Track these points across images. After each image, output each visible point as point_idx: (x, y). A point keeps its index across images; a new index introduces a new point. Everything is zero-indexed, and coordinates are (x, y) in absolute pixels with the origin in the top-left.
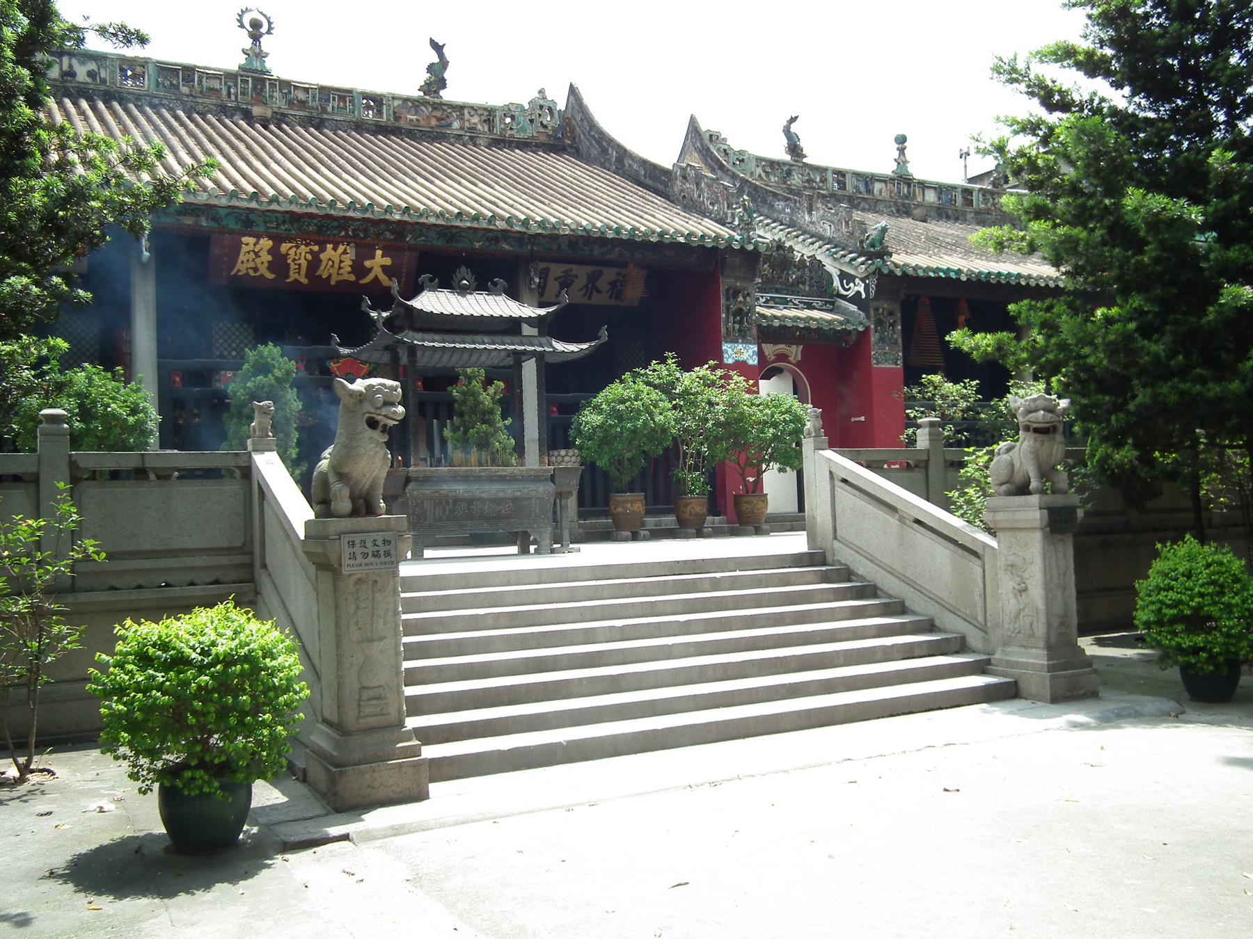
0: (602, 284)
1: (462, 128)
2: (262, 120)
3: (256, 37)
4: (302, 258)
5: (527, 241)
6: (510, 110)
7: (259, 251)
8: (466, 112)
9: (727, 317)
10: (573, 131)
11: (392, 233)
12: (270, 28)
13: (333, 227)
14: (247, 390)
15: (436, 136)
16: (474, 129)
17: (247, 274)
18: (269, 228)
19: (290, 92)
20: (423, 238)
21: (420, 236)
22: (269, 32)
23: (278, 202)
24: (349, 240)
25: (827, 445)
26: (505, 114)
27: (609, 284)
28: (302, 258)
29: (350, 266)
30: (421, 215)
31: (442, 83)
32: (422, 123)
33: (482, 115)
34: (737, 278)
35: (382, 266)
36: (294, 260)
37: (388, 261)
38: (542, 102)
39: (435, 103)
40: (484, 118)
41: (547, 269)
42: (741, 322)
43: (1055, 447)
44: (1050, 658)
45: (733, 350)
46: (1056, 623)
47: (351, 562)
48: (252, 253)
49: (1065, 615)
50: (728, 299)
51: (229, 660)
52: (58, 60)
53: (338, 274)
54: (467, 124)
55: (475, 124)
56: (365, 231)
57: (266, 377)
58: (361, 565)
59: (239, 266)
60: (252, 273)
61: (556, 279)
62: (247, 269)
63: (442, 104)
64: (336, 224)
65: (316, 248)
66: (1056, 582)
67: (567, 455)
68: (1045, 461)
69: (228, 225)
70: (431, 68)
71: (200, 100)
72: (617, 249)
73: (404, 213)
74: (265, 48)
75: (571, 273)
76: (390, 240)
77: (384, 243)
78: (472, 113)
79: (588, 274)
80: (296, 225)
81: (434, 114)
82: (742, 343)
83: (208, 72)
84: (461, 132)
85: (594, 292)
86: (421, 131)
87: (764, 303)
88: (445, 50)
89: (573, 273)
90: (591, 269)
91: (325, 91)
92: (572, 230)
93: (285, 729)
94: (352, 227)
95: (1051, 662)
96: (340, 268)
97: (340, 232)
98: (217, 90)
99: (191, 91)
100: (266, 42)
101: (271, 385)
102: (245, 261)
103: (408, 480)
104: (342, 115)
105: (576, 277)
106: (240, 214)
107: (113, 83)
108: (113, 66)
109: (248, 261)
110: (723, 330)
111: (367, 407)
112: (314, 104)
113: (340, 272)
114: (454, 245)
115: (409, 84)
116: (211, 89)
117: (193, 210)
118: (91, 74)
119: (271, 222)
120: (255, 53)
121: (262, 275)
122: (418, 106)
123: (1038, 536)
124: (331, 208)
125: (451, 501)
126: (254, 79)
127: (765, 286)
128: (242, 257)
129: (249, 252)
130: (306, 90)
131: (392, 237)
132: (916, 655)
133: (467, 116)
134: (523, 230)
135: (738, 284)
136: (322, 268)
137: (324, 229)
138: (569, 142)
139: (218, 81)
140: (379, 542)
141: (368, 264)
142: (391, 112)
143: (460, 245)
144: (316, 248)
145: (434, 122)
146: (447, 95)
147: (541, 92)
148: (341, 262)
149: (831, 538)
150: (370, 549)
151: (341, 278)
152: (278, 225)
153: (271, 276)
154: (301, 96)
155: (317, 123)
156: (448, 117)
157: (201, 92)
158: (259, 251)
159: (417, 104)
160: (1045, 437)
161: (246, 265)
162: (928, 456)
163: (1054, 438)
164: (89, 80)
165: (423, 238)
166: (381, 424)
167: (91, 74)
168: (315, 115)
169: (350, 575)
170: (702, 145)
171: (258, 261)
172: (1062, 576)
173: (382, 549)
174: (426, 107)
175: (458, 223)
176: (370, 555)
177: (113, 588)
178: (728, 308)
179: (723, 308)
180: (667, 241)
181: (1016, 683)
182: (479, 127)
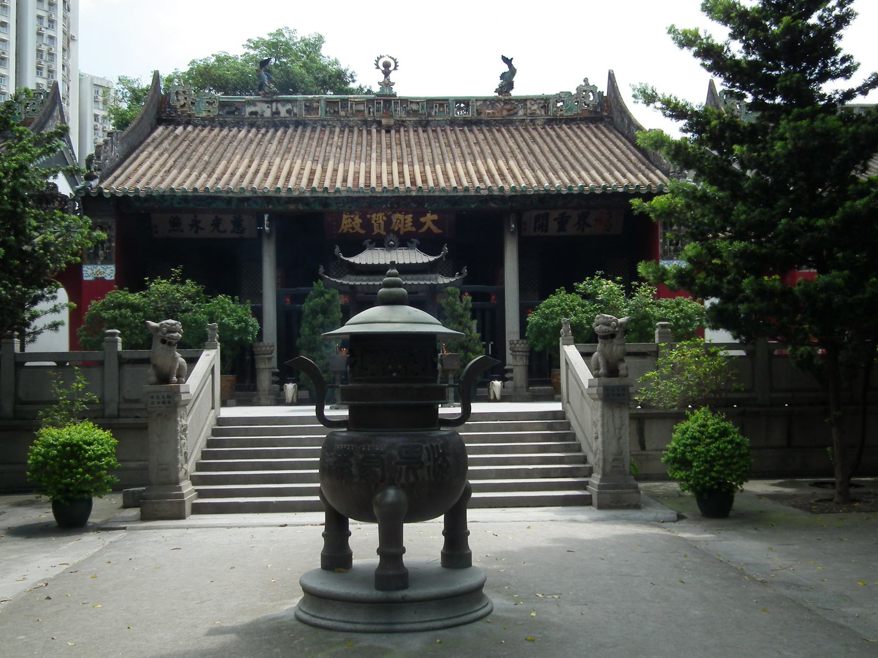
1: (525, 115)
2: (387, 127)
3: (387, 73)
4: (381, 219)
6: (560, 97)
8: (528, 103)
10: (609, 107)
12: (396, 66)
15: (507, 123)
16: (534, 113)
17: (348, 232)
19: (407, 106)
20: (436, 205)
22: (395, 69)
25: (573, 341)
26: (556, 101)
28: (381, 219)
31: (510, 85)
32: (497, 114)
33: (540, 103)
36: (376, 221)
38: (585, 88)
39: (505, 100)
40: (542, 105)
46: (610, 458)
47: (152, 406)
48: (349, 219)
49: (620, 453)
51: (64, 445)
52: (270, 106)
53: (404, 227)
54: (529, 111)
55: (535, 110)
57: (320, 299)
58: (156, 407)
59: (343, 227)
60: (351, 231)
61: (555, 220)
62: (348, 229)
63: (510, 100)
67: (523, 343)
70: (503, 76)
71: (351, 119)
74: (392, 80)
78: (533, 102)
81: (505, 107)
82: (677, 260)
83: (356, 100)
84: (525, 118)
86: (495, 120)
88: (513, 63)
91: (430, 102)
92: (535, 191)
93: (91, 475)
94: (389, 202)
95: (602, 484)
96: (405, 224)
98: (361, 111)
99: (346, 114)
100: (393, 77)
104: (441, 117)
107: (300, 115)
108: (300, 105)
110: (660, 251)
111: (160, 333)
112: (423, 112)
113: (406, 226)
115: (488, 88)
116: (358, 111)
118: (289, 112)
120: (385, 84)
121: (357, 232)
122: (494, 103)
126: (385, 101)
129: (348, 218)
130: (418, 103)
131: (416, 206)
132: (552, 476)
133: (529, 105)
134: (502, 194)
138: (606, 114)
139: (363, 105)
141: (422, 220)
142: (475, 110)
145: (505, 113)
146: (514, 93)
147: (586, 80)
148: (405, 220)
150: (161, 400)
151: (406, 230)
152: (344, 206)
154: (415, 107)
155: (424, 124)
156: (515, 108)
157: (352, 114)
159: (493, 102)
161: (347, 226)
163: (612, 342)
164: (287, 115)
165: (436, 205)
166: (168, 341)
167: (289, 112)
168: (424, 119)
169: (154, 412)
170: (715, 103)
171: (354, 223)
172: (617, 431)
173: (167, 400)
174: (499, 103)
177: (137, 417)
179: (660, 235)
180: (609, 192)
182: (538, 112)
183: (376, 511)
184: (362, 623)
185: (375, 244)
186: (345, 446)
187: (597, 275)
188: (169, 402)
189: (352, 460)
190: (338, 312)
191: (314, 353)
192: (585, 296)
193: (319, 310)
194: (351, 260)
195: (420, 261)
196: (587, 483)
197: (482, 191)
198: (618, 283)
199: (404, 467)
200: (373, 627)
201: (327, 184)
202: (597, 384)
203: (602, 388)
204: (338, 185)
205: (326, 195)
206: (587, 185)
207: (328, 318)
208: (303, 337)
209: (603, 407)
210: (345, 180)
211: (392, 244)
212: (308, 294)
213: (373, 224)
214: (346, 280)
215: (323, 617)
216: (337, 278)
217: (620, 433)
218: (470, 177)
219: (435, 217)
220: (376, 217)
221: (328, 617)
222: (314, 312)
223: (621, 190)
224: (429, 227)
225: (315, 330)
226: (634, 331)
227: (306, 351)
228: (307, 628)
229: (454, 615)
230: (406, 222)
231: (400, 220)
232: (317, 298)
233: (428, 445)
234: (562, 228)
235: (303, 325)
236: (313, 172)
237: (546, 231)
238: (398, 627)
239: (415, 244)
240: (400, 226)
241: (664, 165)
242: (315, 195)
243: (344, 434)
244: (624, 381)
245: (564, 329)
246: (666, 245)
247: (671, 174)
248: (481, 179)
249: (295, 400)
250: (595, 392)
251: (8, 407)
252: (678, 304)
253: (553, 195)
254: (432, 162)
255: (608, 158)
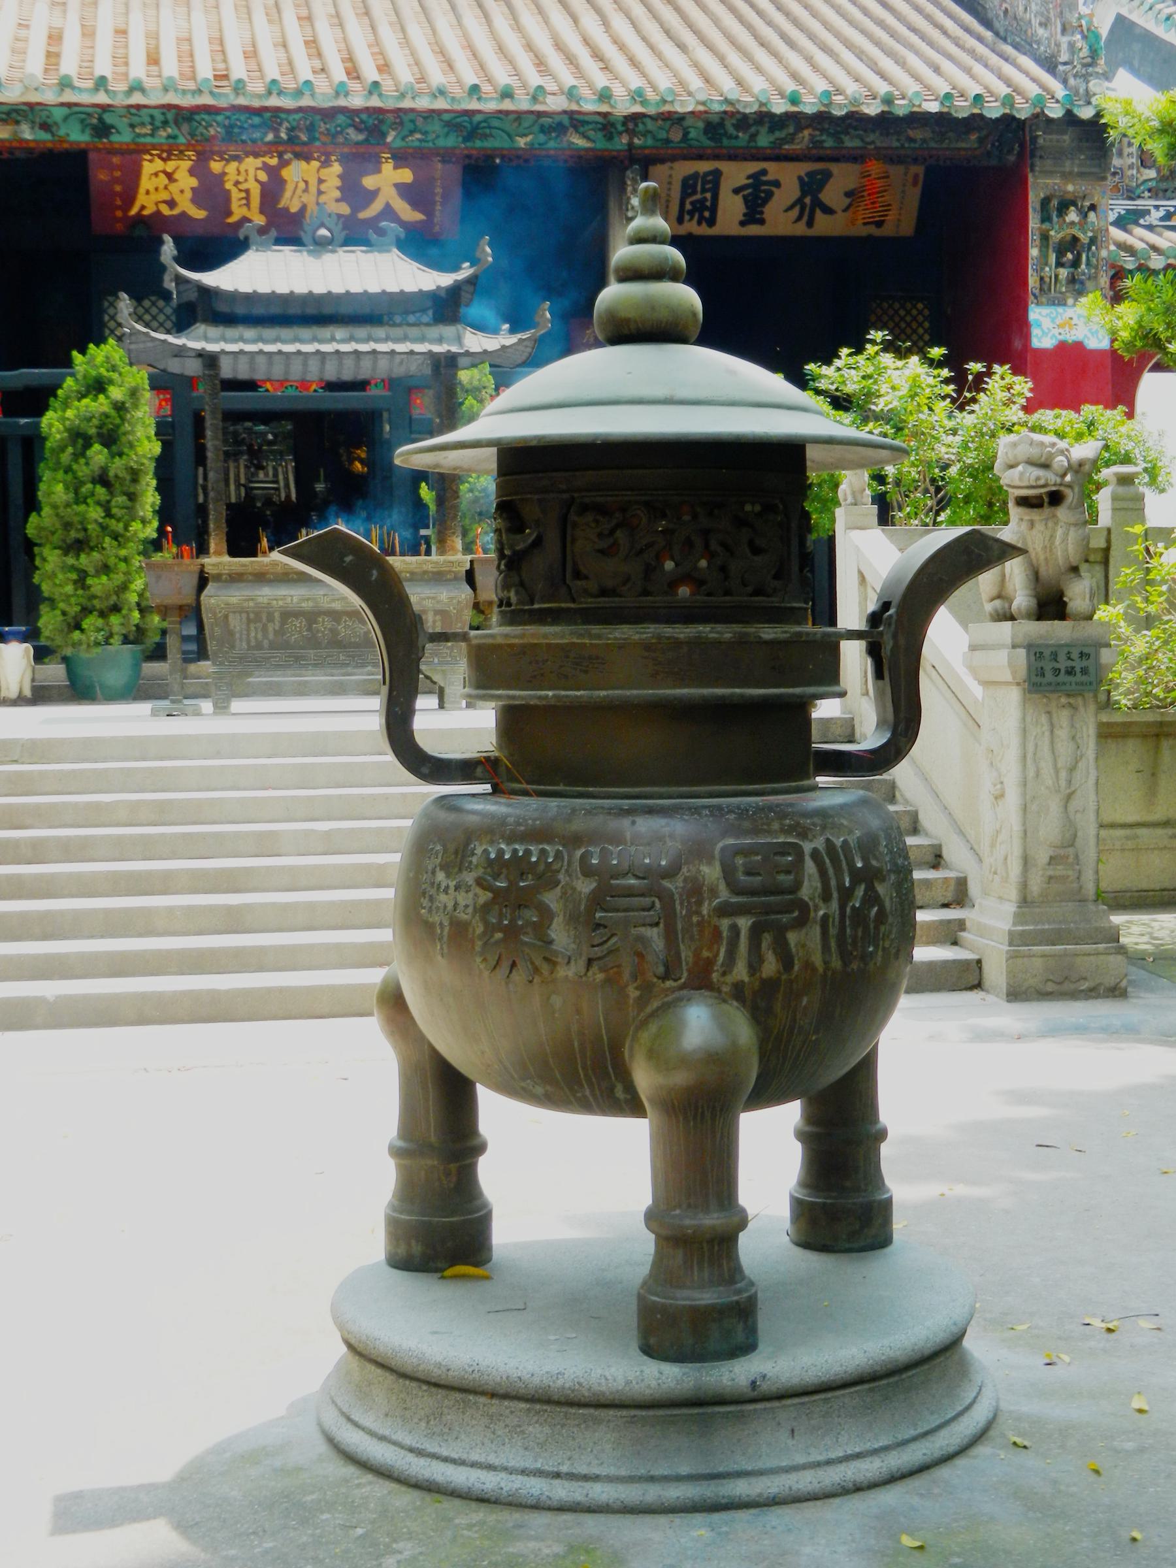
0: (832, 194)
5: (620, 128)
7: (174, 171)
9: (1044, 256)
11: (358, 129)
13: (253, 126)
14: (68, 423)
17: (158, 213)
18: (139, 135)
21: (412, 132)
23: (142, 90)
24: (281, 149)
27: (848, 194)
29: (338, 188)
30: (403, 96)
34: (1067, 176)
35: (396, 185)
36: (237, 183)
37: (406, 175)
41: (717, 174)
42: (1076, 264)
43: (1059, 532)
44: (1019, 918)
45: (1053, 321)
48: (162, 176)
50: (1046, 218)
56: (311, 129)
59: (141, 199)
60: (165, 210)
61: (736, 191)
62: (157, 204)
64: (256, 120)
65: (274, 161)
66: (1049, 782)
68: (1042, 557)
69: (68, 135)
72: (806, 133)
73: (370, 93)
75: (764, 178)
76: (357, 144)
77: (346, 150)
79: (800, 178)
80: (185, 128)
85: (818, 212)
87: (1162, 219)
89: (769, 177)
90: (804, 168)
94: (286, 125)
96: (320, 193)
97: (265, 134)
101: (107, 416)
102: (152, 190)
103: (203, 581)
105: (777, 184)
106: (88, 114)
109: (157, 189)
110: (1033, 281)
114: (478, 144)
117: (8, 114)
119: (143, 124)
121: (184, 214)
123: (1014, 695)
124: (237, 94)
125: (277, 615)
127: (1164, 185)
128: (146, 183)
129: (156, 174)
134: (604, 108)
135: (1070, 188)
136: (288, 194)
137: (236, 130)
140: (1075, 655)
141: (369, 182)
143: (489, 144)
144: (274, 161)
148: (321, 181)
149: (859, 691)
150: (1063, 664)
152: (155, 130)
153: (199, 214)
158: (174, 171)
160: (1035, 515)
161: (155, 197)
162: (1108, 541)
165: (418, 136)
171: (173, 188)
175: (474, 105)
176: (1063, 671)
178: (1045, 237)
179: (1033, 236)
181: (979, 962)
183: (644, 1079)
184: (610, 1479)
185: (273, 233)
186: (521, 849)
187: (873, 342)
188: (1084, 671)
189: (551, 899)
190: (148, 438)
191: (83, 556)
192: (840, 402)
193: (92, 431)
194: (209, 279)
195: (411, 287)
196: (961, 925)
197: (550, 100)
198: (932, 363)
199: (744, 923)
200: (652, 1493)
201: (104, 67)
202: (1009, 641)
203: (1022, 652)
204: (138, 70)
205: (102, 98)
206: (839, 91)
207: (120, 454)
208: (46, 511)
209: (1025, 701)
210: (153, 60)
211: (325, 237)
212: (59, 386)
213: (228, 193)
214: (197, 339)
215: (455, 1455)
216: (168, 332)
217: (1069, 782)
218: (511, 62)
219: (406, 175)
220: (239, 173)
221: (475, 1457)
222: (80, 439)
223: (933, 107)
224: (388, 205)
225: (83, 490)
226: (967, 500)
227: (58, 552)
228: (405, 1498)
229: (912, 1433)
230: (323, 187)
231: (306, 182)
232: (84, 396)
233: (819, 843)
234: (753, 214)
235: (46, 475)
236: (55, 37)
237: (712, 222)
238: (741, 1488)
239: (391, 237)
240: (305, 199)
241: (1039, 43)
242: (69, 97)
243: (478, 806)
244: (1085, 631)
245: (851, 485)
246: (1046, 264)
247: (1061, 68)
248: (541, 64)
249: (28, 692)
250: (1005, 661)
251: (1166, 755)
252: (1091, 425)
253: (745, 117)
254: (394, 18)
255: (881, 24)
